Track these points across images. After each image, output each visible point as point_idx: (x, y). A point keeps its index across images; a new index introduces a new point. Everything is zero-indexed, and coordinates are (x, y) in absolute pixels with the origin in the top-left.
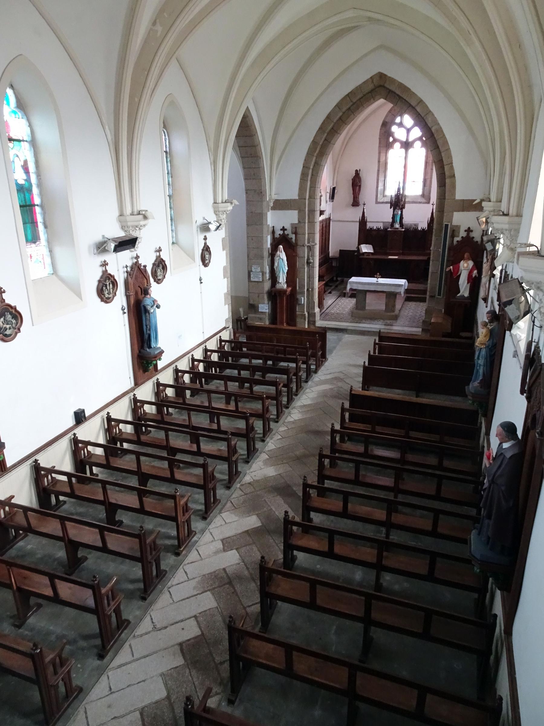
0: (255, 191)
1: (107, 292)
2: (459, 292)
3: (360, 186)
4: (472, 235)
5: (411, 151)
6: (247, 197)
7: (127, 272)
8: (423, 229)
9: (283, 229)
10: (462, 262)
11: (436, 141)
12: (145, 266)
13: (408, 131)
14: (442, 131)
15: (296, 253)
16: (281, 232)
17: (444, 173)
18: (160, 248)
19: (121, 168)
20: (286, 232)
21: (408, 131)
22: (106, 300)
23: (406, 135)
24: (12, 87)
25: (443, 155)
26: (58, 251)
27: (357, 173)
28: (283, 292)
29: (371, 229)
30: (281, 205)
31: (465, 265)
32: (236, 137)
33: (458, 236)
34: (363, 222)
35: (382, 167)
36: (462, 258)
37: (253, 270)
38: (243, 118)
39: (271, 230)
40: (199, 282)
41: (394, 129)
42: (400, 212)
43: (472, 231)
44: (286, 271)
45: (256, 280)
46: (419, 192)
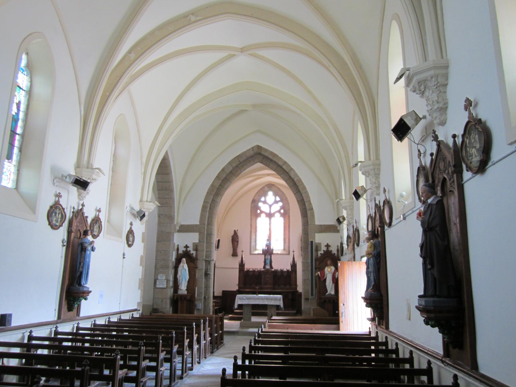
0: (166, 215)
1: (55, 219)
2: (327, 292)
3: (238, 242)
4: (330, 249)
5: (273, 219)
6: (159, 220)
7: (73, 212)
8: (288, 270)
9: (187, 247)
10: (326, 269)
11: (298, 187)
12: (87, 217)
13: (270, 206)
14: (301, 181)
15: (196, 265)
16: (184, 249)
17: (306, 208)
18: (100, 209)
19: (85, 140)
20: (188, 249)
21: (270, 206)
22: (54, 227)
23: (269, 209)
24: (27, 54)
25: (303, 195)
26: (25, 172)
27: (235, 233)
28: (182, 297)
29: (248, 271)
30: (185, 229)
31: (329, 270)
32: (156, 174)
33: (320, 250)
34: (242, 265)
35: (253, 229)
36: (326, 265)
37: (159, 278)
38: (163, 160)
39: (176, 247)
40: (122, 257)
41: (260, 204)
42: (269, 257)
43: (330, 246)
44: (187, 280)
45: (161, 286)
46: (281, 247)
